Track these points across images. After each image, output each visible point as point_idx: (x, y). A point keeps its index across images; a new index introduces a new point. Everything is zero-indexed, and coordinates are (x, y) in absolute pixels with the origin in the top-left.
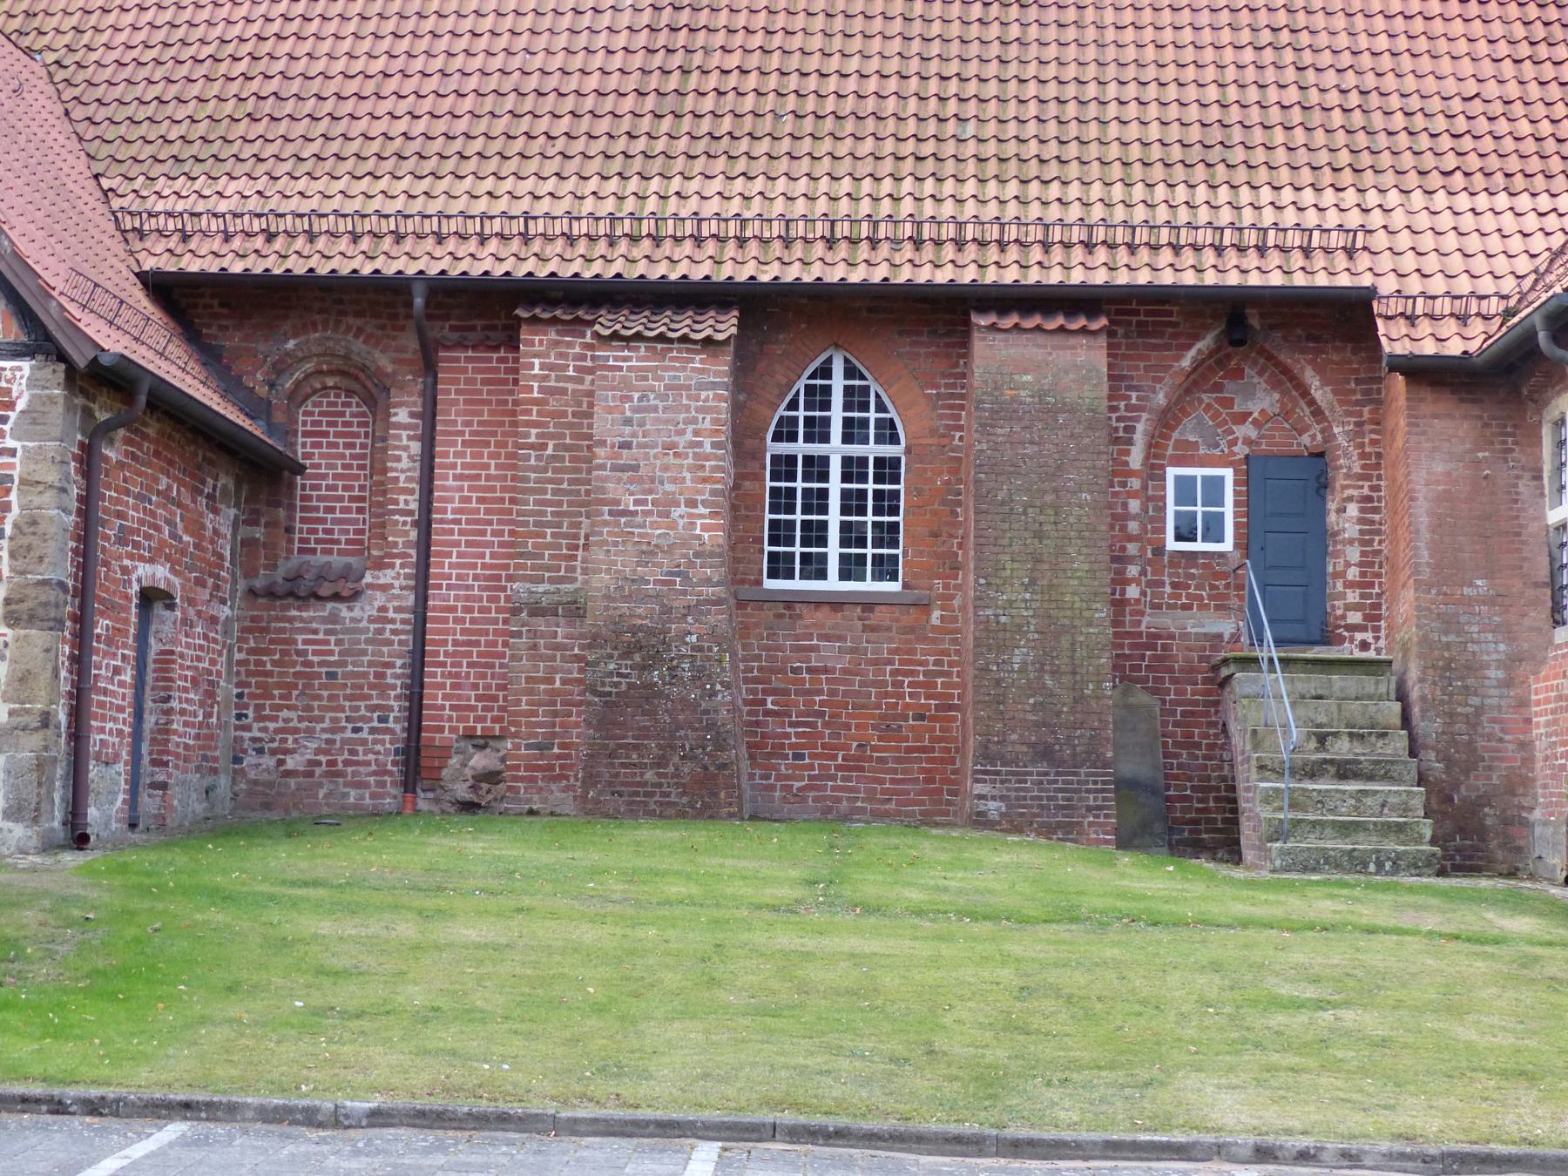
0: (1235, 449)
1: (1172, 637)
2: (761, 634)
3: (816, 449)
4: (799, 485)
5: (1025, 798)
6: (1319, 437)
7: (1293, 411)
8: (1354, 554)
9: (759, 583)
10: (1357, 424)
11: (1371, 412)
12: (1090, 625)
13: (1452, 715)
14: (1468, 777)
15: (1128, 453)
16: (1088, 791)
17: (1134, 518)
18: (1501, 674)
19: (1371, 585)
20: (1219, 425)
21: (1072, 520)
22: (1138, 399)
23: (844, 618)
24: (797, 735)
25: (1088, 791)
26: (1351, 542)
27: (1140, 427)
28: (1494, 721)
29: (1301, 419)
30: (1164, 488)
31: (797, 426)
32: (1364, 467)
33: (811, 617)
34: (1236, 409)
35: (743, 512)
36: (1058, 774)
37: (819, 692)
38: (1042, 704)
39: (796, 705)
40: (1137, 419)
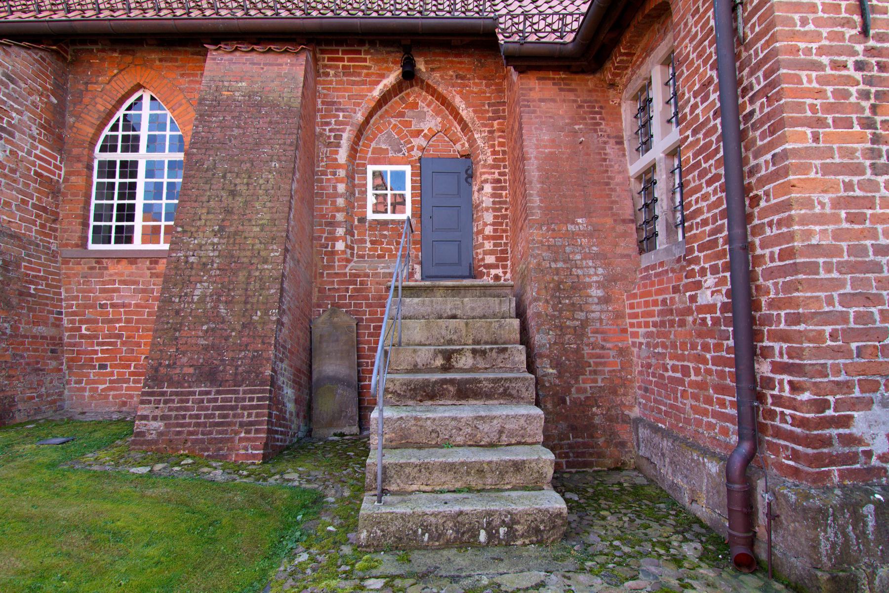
0: (412, 153)
1: (367, 275)
2: (79, 282)
3: (129, 156)
4: (117, 180)
5: (184, 417)
6: (467, 145)
7: (450, 128)
8: (489, 217)
9: (84, 245)
10: (489, 132)
11: (499, 124)
12: (265, 261)
13: (561, 328)
14: (577, 382)
15: (337, 153)
16: (244, 408)
17: (341, 196)
18: (600, 293)
19: (501, 238)
20: (401, 138)
21: (261, 181)
22: (344, 117)
23: (137, 268)
24: (103, 351)
25: (244, 408)
26: (487, 209)
27: (345, 136)
28: (596, 332)
29: (455, 134)
30: (365, 179)
31: (117, 141)
32: (494, 160)
33: (114, 269)
34: (413, 128)
35: (69, 197)
36: (218, 392)
37: (119, 321)
38: (213, 330)
39: (103, 330)
40: (343, 130)
